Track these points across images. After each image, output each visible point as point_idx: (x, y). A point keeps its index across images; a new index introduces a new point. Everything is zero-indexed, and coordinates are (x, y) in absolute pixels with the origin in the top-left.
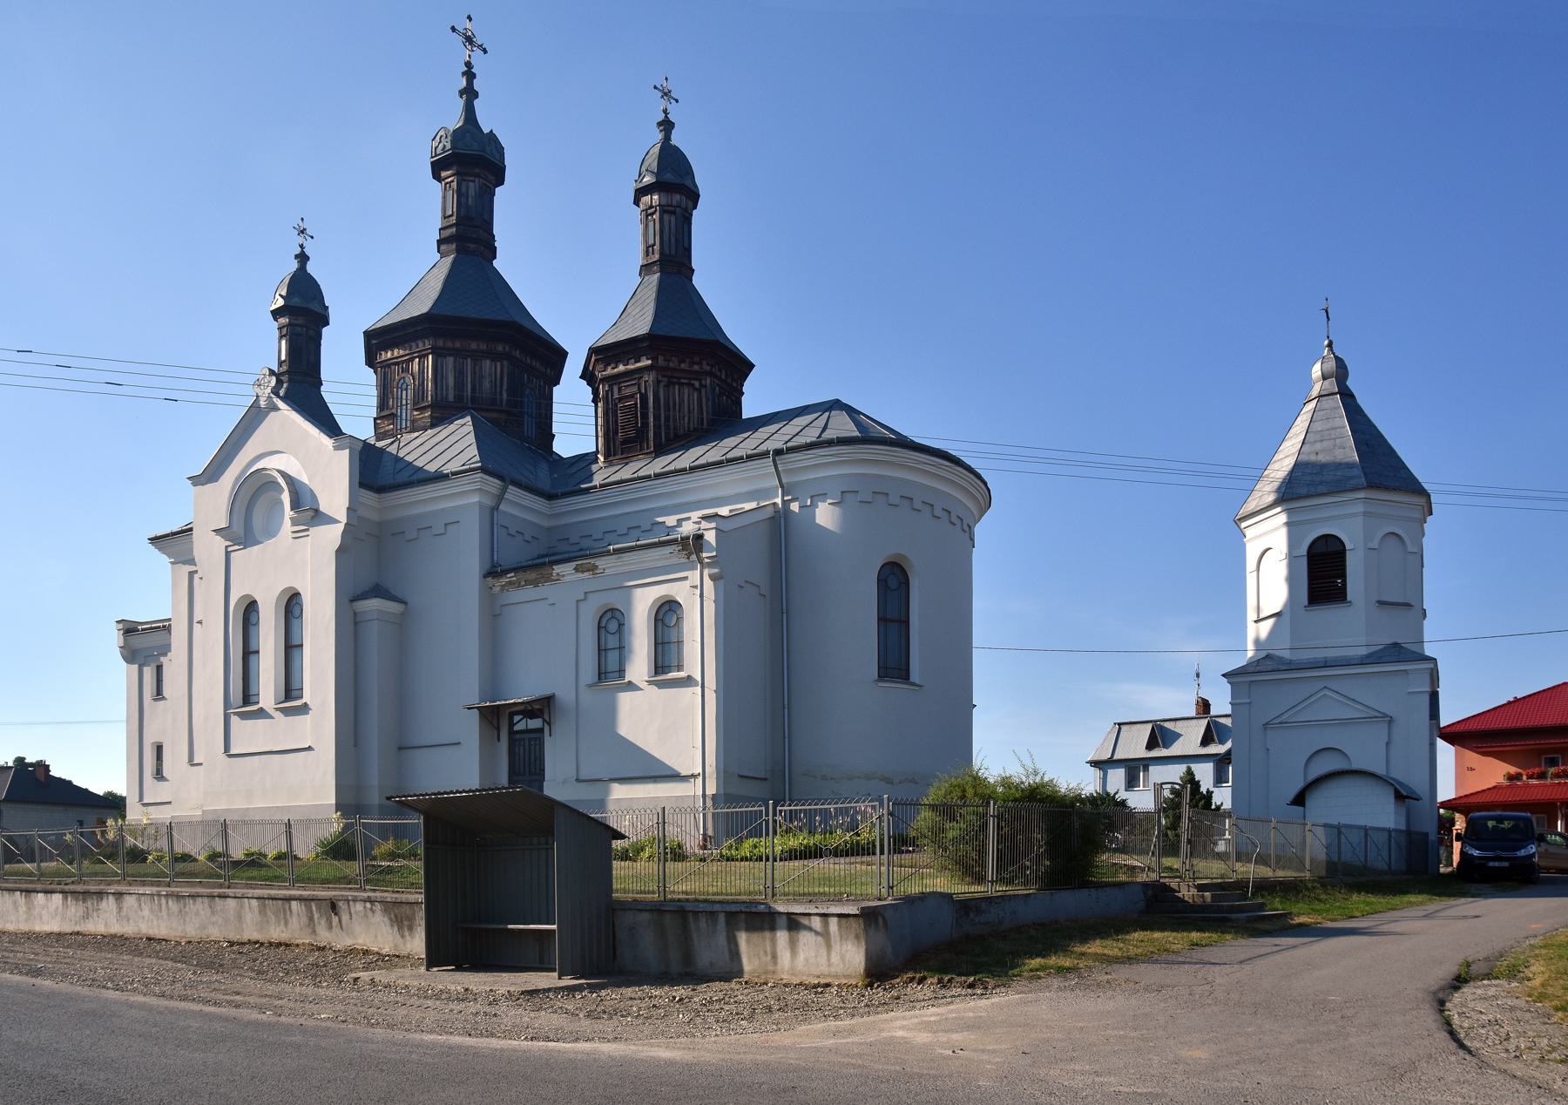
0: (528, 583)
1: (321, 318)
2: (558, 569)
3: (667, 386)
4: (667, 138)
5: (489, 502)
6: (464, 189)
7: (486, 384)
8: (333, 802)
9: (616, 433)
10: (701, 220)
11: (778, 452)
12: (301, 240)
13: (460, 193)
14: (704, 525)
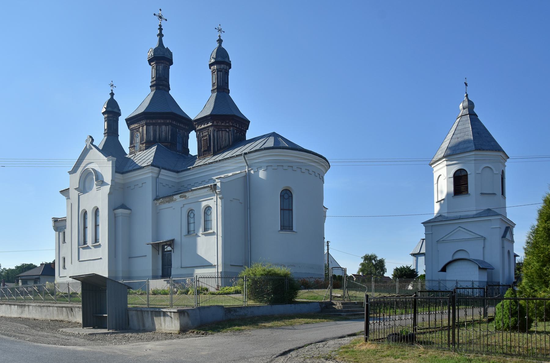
0: (167, 202)
2: (175, 197)
3: (217, 131)
4: (220, 45)
5: (155, 175)
7: (164, 134)
10: (232, 74)
11: (246, 154)
12: (111, 88)
13: (157, 70)
14: (217, 181)
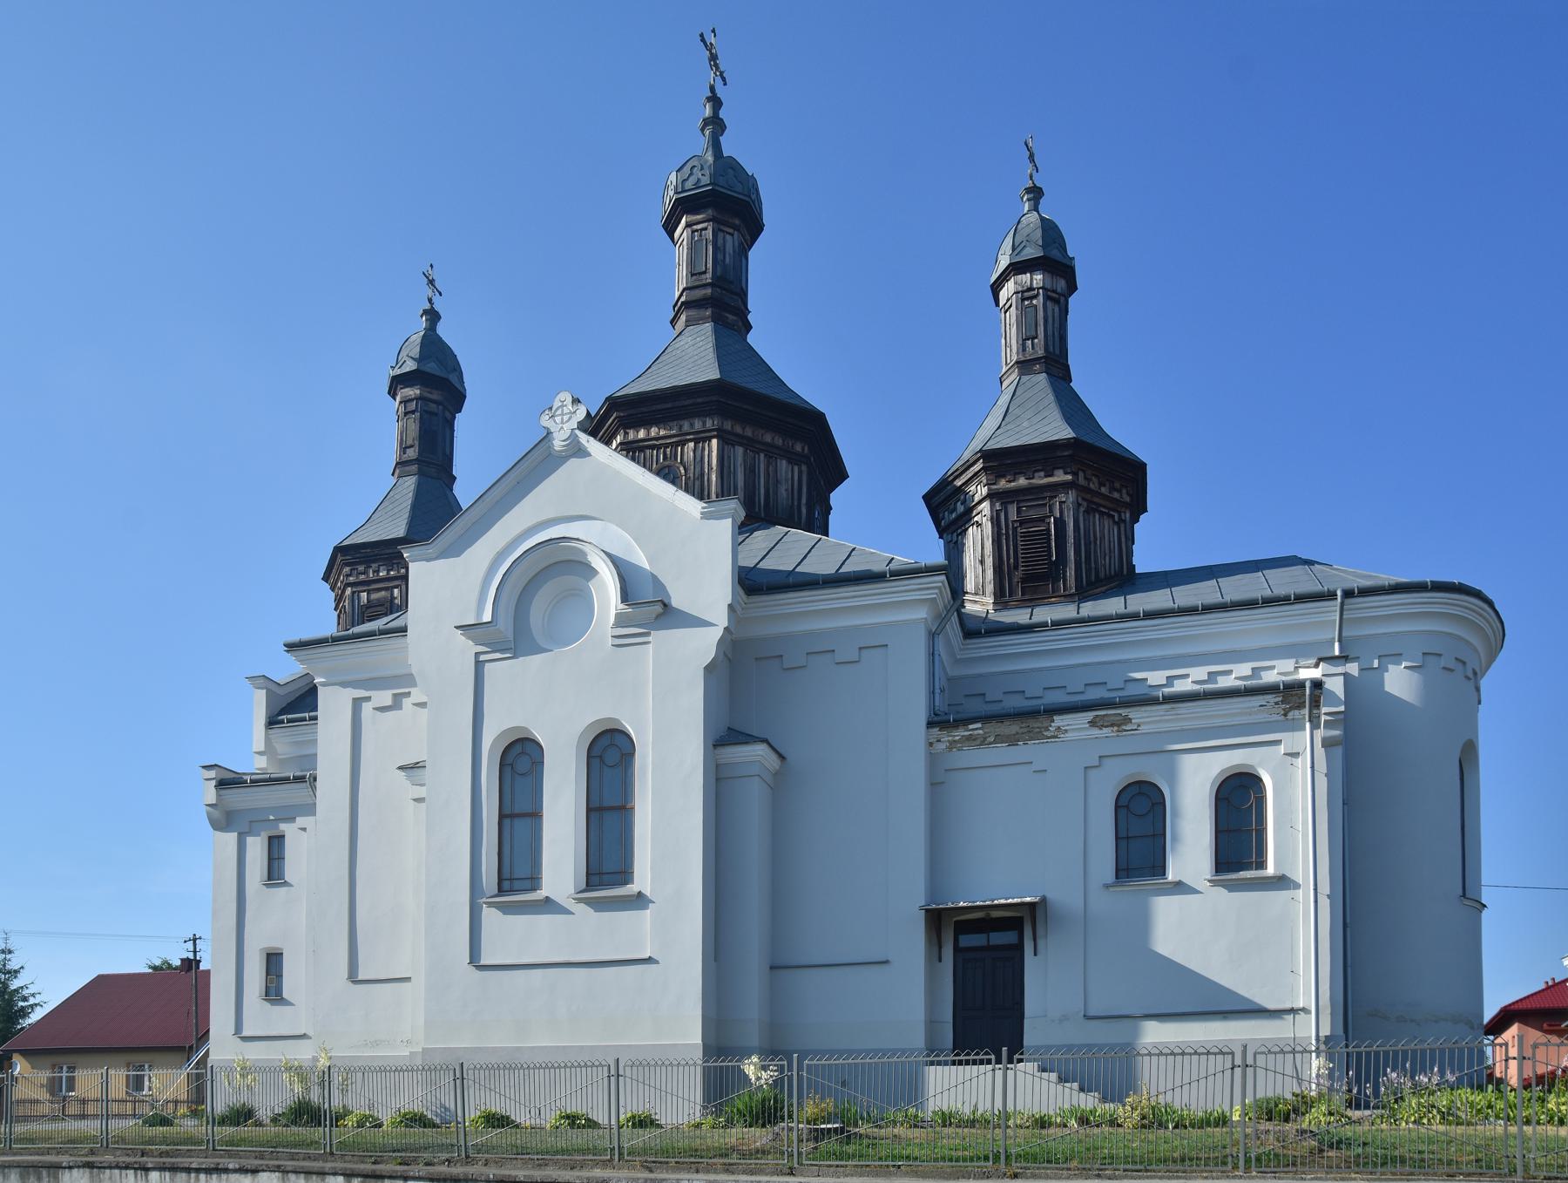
0: (999, 739)
1: (456, 398)
3: (1087, 512)
6: (720, 242)
8: (697, 1039)
9: (1016, 568)
